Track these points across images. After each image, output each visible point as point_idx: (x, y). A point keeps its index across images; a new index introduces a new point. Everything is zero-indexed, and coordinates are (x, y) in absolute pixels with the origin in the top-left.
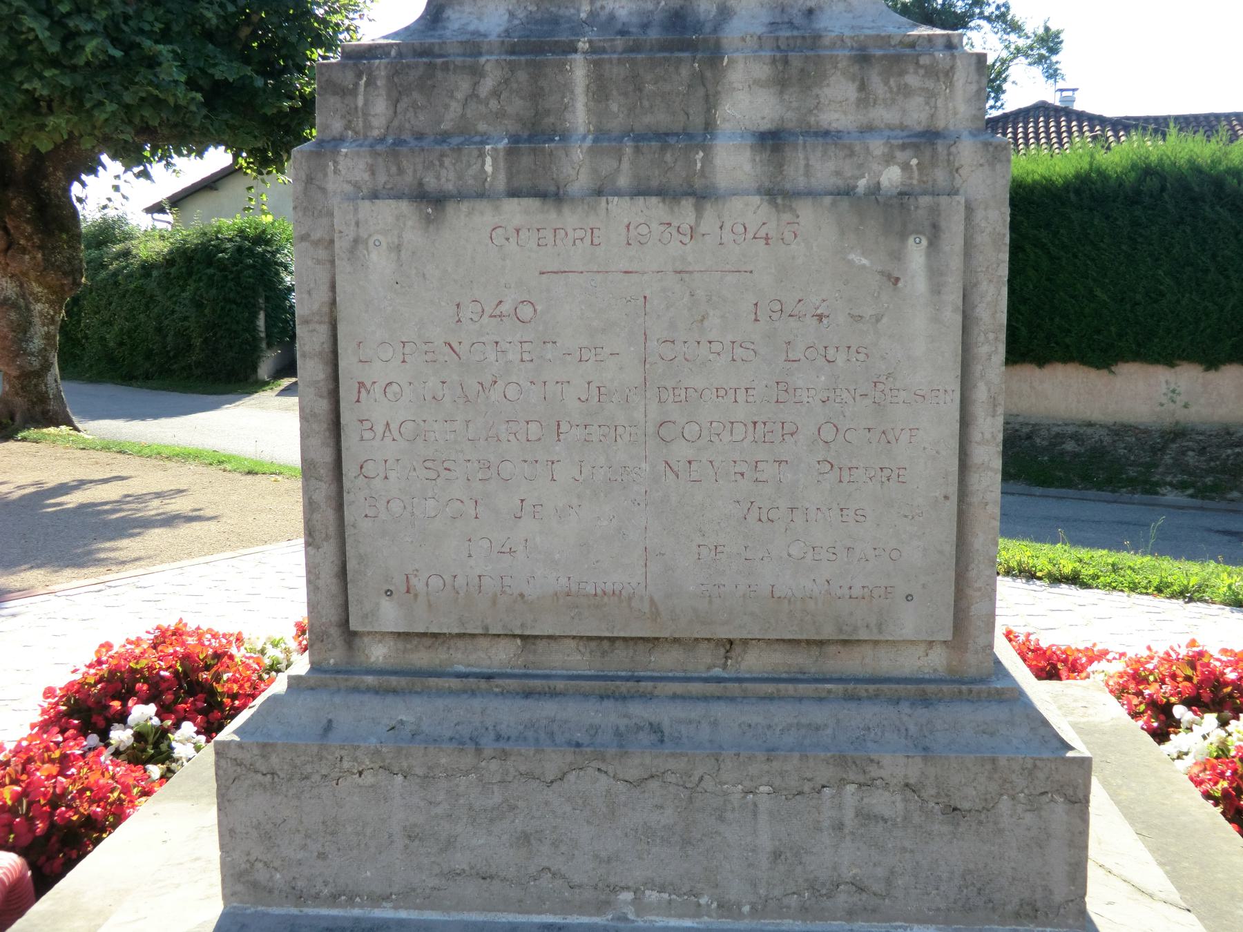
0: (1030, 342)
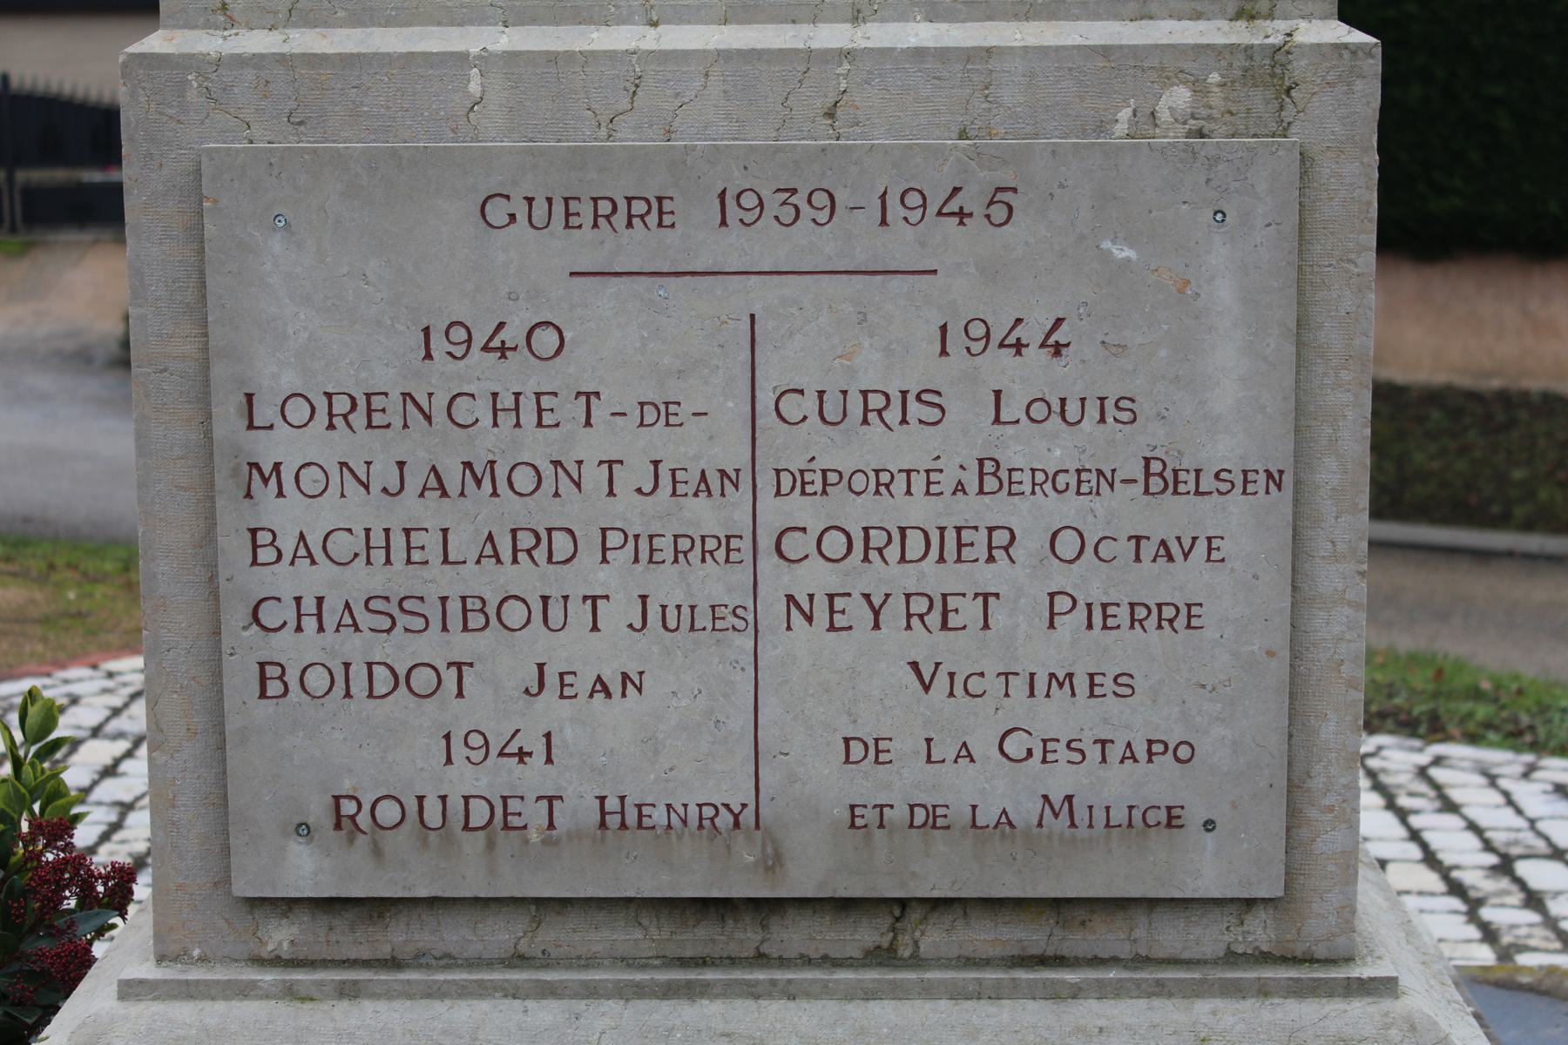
0: (1377, 513)
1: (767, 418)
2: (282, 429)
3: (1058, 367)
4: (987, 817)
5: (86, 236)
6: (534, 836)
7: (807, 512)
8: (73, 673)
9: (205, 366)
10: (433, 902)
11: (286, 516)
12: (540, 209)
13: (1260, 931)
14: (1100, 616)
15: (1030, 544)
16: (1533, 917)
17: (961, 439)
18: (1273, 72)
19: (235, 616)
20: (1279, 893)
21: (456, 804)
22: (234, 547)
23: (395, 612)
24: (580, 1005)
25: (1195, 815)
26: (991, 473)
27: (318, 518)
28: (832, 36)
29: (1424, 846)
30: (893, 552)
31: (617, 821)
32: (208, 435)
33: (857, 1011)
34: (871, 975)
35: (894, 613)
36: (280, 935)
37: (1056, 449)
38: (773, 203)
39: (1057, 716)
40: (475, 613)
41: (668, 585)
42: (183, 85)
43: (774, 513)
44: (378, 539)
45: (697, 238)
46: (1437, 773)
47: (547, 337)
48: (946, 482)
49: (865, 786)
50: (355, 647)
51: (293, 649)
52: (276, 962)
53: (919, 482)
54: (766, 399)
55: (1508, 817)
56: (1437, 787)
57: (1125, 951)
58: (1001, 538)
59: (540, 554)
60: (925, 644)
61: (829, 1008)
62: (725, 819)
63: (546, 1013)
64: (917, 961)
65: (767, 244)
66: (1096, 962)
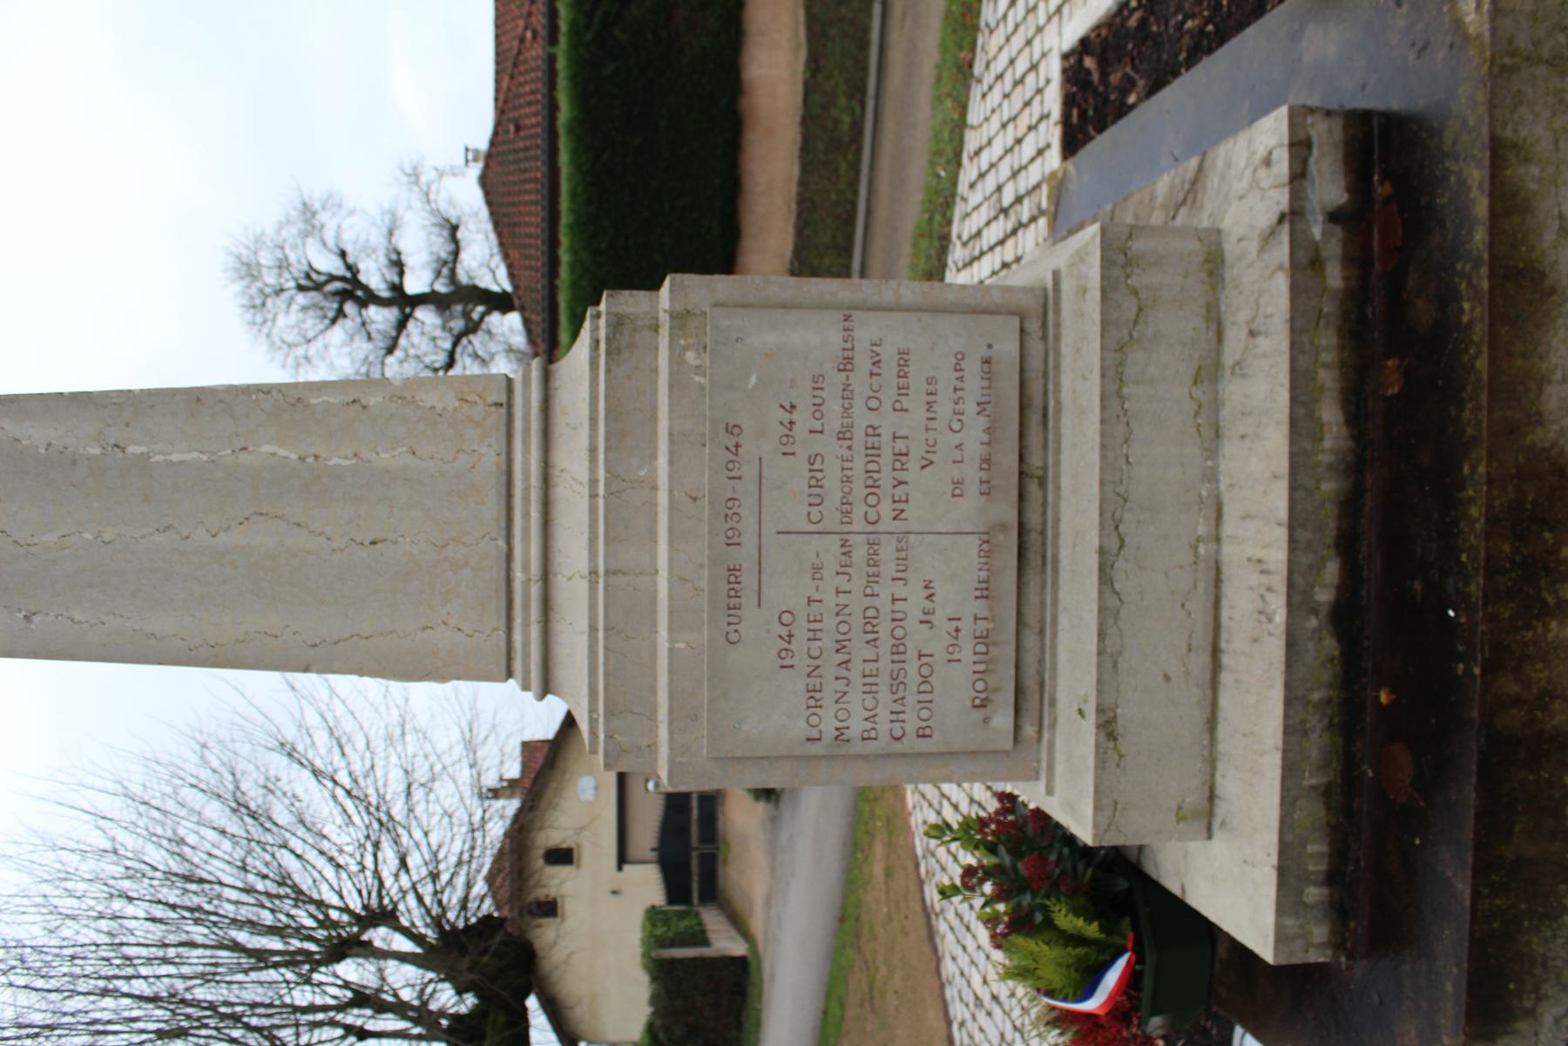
1: (819, 527)
2: (822, 727)
3: (801, 406)
4: (985, 438)
5: (721, 817)
6: (991, 626)
7: (858, 512)
8: (913, 822)
9: (796, 757)
10: (1017, 667)
11: (857, 726)
12: (732, 620)
13: (1033, 326)
14: (903, 390)
15: (873, 419)
16: (1026, 202)
17: (829, 447)
18: (681, 318)
19: (898, 747)
20: (1017, 319)
21: (977, 658)
22: (869, 747)
23: (897, 682)
24: (1061, 607)
25: (985, 352)
26: (844, 435)
27: (858, 713)
28: (663, 498)
29: (996, 245)
30: (876, 476)
31: (985, 592)
32: (824, 757)
33: (1065, 493)
34: (1050, 487)
35: (900, 475)
36: (1029, 730)
37: (834, 407)
38: (731, 524)
39: (944, 408)
40: (898, 649)
41: (888, 569)
42: (681, 764)
43: (858, 525)
44: (867, 688)
45: (745, 555)
46: (965, 237)
47: (785, 618)
48: (847, 454)
49: (972, 488)
50: (911, 699)
51: (912, 725)
52: (1040, 732)
53: (847, 465)
54: (812, 528)
55: (984, 209)
56: (971, 238)
57: (1041, 382)
58: (870, 431)
59: (875, 622)
60: (914, 463)
61: (1064, 505)
62: (985, 547)
63: (1063, 621)
64: (1045, 468)
65: (748, 526)
66: (1046, 393)
